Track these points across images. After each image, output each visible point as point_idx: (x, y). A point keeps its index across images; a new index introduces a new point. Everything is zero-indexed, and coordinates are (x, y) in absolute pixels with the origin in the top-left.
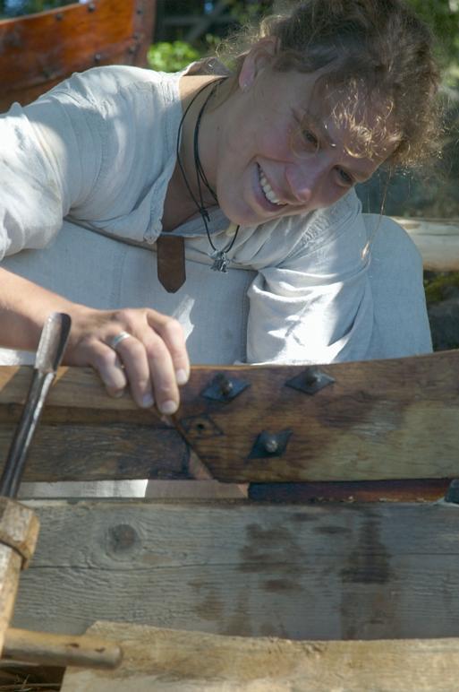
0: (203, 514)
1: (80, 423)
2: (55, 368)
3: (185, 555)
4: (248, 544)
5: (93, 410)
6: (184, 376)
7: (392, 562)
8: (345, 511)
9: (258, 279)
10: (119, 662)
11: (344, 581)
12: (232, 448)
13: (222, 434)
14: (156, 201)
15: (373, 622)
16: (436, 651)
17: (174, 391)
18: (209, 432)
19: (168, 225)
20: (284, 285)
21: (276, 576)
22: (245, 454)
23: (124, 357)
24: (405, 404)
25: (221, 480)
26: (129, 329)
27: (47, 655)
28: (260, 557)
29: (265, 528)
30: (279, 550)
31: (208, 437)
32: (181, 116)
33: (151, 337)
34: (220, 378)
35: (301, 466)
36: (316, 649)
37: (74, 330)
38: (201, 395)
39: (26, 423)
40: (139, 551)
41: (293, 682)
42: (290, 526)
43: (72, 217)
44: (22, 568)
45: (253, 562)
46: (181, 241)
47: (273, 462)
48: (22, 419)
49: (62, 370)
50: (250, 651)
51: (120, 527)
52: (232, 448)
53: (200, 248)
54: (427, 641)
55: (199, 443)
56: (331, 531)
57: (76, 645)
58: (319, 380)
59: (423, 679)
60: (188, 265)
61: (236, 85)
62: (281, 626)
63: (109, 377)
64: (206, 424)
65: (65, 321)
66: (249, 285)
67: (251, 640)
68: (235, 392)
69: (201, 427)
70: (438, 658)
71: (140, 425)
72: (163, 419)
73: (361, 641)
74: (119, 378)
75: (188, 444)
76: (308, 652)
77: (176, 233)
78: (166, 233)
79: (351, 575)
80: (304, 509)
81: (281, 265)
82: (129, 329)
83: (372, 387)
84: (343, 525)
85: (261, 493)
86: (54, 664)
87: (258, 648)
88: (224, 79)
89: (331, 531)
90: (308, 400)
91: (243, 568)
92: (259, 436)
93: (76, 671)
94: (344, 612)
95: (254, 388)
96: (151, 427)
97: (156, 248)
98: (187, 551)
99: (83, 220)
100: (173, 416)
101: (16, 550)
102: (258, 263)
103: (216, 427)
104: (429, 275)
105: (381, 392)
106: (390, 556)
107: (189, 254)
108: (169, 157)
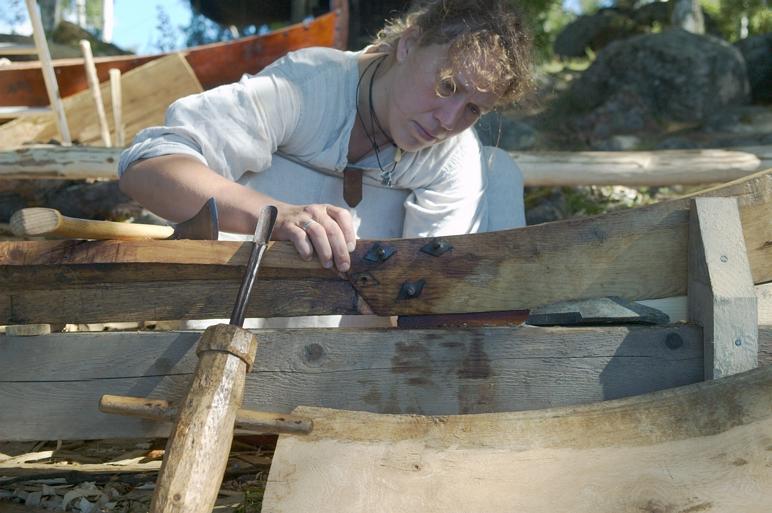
0: (367, 336)
1: (285, 278)
2: (267, 242)
3: (355, 363)
4: (397, 355)
5: (291, 269)
6: (353, 247)
7: (492, 364)
8: (461, 332)
9: (411, 196)
10: (311, 429)
11: (460, 378)
12: (387, 293)
13: (379, 283)
14: (344, 141)
15: (480, 403)
16: (519, 419)
17: (347, 256)
18: (370, 283)
19: (352, 159)
20: (427, 201)
21: (415, 375)
22: (395, 296)
23: (311, 237)
24: (499, 261)
25: (379, 315)
26: (314, 217)
27: (264, 426)
28: (405, 363)
29: (407, 344)
30: (416, 359)
31: (368, 287)
32: (358, 79)
33: (330, 221)
34: (376, 246)
35: (431, 304)
36: (441, 421)
37: (279, 218)
38: (364, 258)
39: (248, 278)
40: (323, 361)
41: (426, 441)
42: (423, 343)
43: (281, 152)
44: (247, 371)
45: (400, 367)
46: (360, 173)
47: (413, 302)
48: (245, 276)
49: (271, 243)
50: (398, 423)
51: (312, 345)
52: (386, 293)
53: (373, 172)
54: (513, 413)
55: (364, 290)
56: (451, 345)
57: (282, 420)
58: (442, 246)
59: (510, 437)
60: (365, 188)
61: (395, 59)
62: (420, 408)
63: (301, 247)
64: (368, 277)
65: (273, 211)
66: (404, 200)
67: (399, 416)
68: (387, 256)
69: (365, 279)
70: (520, 423)
71: (324, 279)
72: (340, 275)
73: (267, 68)
74: (307, 247)
75: (356, 291)
76: (436, 422)
77: (357, 166)
78: (351, 166)
79: (465, 374)
80: (432, 332)
81: (427, 188)
82: (314, 217)
83: (478, 251)
84: (459, 341)
85: (406, 322)
86: (269, 432)
87: (403, 421)
88: (385, 56)
89: (451, 345)
90: (435, 260)
91: (394, 370)
92: (403, 284)
93: (285, 437)
94: (460, 397)
95: (399, 253)
96: (331, 280)
97: (343, 176)
98: (356, 360)
99: (292, 155)
100: (346, 273)
101: (242, 359)
102: (412, 186)
103: (374, 279)
104: (527, 190)
105: (484, 254)
106: (490, 361)
107: (365, 180)
108: (350, 111)
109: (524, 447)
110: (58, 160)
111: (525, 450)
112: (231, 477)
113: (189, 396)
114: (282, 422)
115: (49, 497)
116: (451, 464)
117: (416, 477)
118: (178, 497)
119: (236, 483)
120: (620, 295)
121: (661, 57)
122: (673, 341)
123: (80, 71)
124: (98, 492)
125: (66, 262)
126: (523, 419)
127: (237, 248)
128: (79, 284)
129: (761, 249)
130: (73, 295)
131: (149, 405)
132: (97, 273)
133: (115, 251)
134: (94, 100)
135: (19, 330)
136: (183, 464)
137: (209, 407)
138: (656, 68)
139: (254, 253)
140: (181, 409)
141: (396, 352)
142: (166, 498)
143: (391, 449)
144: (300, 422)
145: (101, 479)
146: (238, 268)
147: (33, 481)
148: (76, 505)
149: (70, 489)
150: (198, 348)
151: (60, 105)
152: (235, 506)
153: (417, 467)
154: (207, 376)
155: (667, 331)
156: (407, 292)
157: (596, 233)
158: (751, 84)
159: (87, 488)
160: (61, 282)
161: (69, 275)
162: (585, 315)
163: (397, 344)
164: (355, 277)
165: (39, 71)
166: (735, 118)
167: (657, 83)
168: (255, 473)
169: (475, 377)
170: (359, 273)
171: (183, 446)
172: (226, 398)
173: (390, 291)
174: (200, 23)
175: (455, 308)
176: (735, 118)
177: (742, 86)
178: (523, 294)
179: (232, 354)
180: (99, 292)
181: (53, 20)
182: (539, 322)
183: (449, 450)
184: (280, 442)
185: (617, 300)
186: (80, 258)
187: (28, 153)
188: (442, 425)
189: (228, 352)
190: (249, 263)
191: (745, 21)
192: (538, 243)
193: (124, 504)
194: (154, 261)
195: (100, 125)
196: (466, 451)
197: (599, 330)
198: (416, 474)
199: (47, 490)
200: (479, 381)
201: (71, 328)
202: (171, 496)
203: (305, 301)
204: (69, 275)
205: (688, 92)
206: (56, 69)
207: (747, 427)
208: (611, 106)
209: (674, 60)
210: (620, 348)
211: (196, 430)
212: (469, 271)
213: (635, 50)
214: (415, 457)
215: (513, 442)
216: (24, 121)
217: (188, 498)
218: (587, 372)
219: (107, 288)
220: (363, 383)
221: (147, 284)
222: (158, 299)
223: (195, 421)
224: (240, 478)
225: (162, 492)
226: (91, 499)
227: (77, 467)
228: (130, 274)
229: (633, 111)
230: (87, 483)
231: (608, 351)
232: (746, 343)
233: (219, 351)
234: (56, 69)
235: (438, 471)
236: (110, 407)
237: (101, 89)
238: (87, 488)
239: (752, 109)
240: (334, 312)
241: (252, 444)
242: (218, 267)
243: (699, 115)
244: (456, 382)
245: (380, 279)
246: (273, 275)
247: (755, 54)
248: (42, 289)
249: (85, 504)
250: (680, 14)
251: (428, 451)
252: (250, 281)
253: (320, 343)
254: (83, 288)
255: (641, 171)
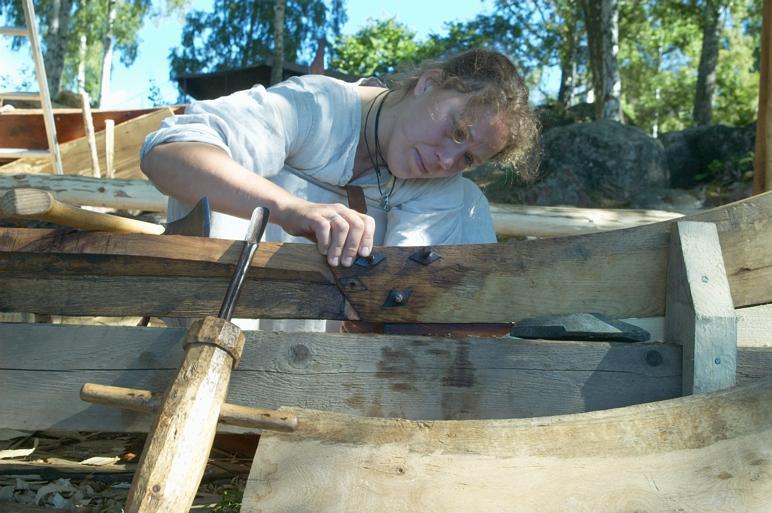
16: (504, 427)
22: (381, 303)
24: (486, 273)
28: (391, 368)
29: (393, 350)
30: (402, 364)
35: (417, 313)
36: (426, 426)
42: (410, 349)
45: (385, 372)
47: (401, 310)
48: (236, 273)
50: (383, 426)
51: (298, 346)
55: (352, 295)
56: (437, 352)
57: (268, 415)
62: (402, 413)
64: (357, 282)
69: (353, 284)
70: (506, 430)
71: (312, 282)
75: (344, 295)
79: (449, 381)
80: (420, 338)
84: (445, 349)
89: (437, 352)
91: (379, 375)
101: (229, 353)
103: (363, 285)
106: (474, 369)
109: (509, 454)
110: (51, 187)
111: (510, 457)
112: (209, 481)
113: (174, 387)
114: (267, 418)
115: (23, 491)
116: (435, 469)
117: (399, 480)
118: (157, 488)
119: (211, 486)
120: (602, 313)
121: (595, 143)
122: (653, 358)
123: (78, 119)
124: (72, 489)
125: (53, 251)
126: (509, 426)
127: (228, 247)
128: (66, 275)
129: (736, 274)
130: (60, 287)
131: (132, 395)
132: (86, 264)
133: (104, 243)
134: (89, 145)
135: (3, 317)
136: (165, 454)
137: (193, 399)
138: (590, 152)
139: (246, 249)
140: (164, 400)
141: (383, 356)
142: (144, 489)
143: (375, 451)
144: (286, 419)
145: (77, 477)
146: (227, 266)
147: (7, 476)
148: (49, 500)
149: (43, 484)
150: (185, 341)
151: (57, 149)
152: (212, 505)
153: (401, 470)
154: (193, 368)
155: (649, 348)
156: (394, 300)
157: (580, 251)
158: (671, 173)
159: (62, 484)
160: (48, 271)
161: (57, 265)
162: (569, 329)
163: (383, 349)
164: (343, 282)
165: (40, 118)
166: (659, 197)
167: (591, 165)
168: (232, 478)
169: (460, 385)
170: (347, 278)
171: (164, 437)
172: (211, 391)
173: (379, 298)
174: (186, 101)
175: (440, 318)
176: (659, 197)
177: (665, 174)
178: (507, 307)
179: (219, 347)
180: (86, 284)
181: (57, 89)
182: (525, 335)
183: (433, 455)
184: (262, 441)
185: (599, 316)
186: (70, 247)
187: (25, 179)
188: (427, 430)
189: (215, 345)
190: (240, 261)
191: (655, 128)
192: (524, 257)
193: (99, 501)
194: (145, 255)
195: (93, 168)
196: (450, 456)
197: (582, 344)
198: (400, 477)
199: (21, 484)
200: (463, 389)
201: (57, 321)
202: (150, 487)
203: (292, 304)
204: (57, 265)
205: (617, 174)
206: (56, 116)
207: (731, 442)
208: (551, 182)
209: (606, 146)
210: (602, 362)
211: (179, 421)
212: (457, 282)
213: (573, 135)
214: (400, 460)
215: (499, 449)
216: (23, 162)
217: (167, 492)
218: (569, 385)
219: (95, 280)
220: (348, 386)
221: (135, 278)
222: (146, 294)
223: (178, 412)
224: (217, 482)
225: (140, 482)
226: (65, 495)
227: (55, 462)
228: (118, 267)
229: (570, 188)
230: (61, 480)
231: (590, 365)
232: (726, 362)
233: (206, 343)
234: (56, 116)
235: (422, 475)
236: (91, 396)
237: (96, 136)
238: (62, 484)
239: (674, 192)
240: (320, 317)
241: (228, 452)
242: (207, 265)
243: (627, 195)
244: (438, 386)
245: (368, 285)
246: (261, 276)
247: (673, 146)
248: (29, 278)
249: (58, 500)
250: (608, 112)
251: (413, 455)
252: (240, 278)
253: (306, 345)
254: (70, 279)
255: (591, 225)
